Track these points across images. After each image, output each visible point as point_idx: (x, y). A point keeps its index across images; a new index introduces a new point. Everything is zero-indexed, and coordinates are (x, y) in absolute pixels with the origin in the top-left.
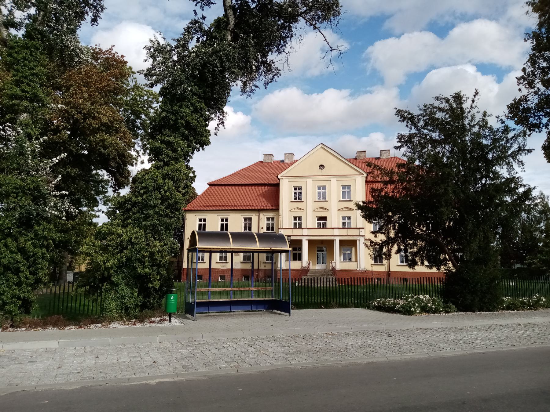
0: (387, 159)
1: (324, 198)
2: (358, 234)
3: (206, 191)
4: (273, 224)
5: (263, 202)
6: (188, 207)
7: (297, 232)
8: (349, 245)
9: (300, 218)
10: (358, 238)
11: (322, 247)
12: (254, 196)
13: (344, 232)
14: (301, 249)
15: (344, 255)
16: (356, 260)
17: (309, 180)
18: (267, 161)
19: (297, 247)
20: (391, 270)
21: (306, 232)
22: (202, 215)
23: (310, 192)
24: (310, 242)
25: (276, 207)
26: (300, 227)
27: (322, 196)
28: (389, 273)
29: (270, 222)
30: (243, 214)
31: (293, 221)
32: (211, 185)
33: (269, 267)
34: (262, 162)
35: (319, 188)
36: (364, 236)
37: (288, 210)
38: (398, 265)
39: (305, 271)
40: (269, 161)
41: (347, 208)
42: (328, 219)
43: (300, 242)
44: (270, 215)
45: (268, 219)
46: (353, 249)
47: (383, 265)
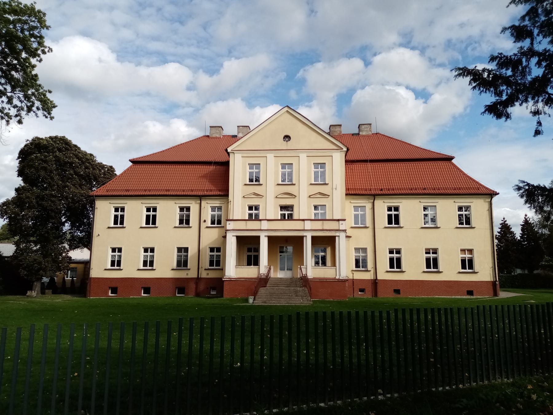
0: (368, 136)
1: (291, 180)
2: (337, 228)
3: (128, 169)
4: (220, 217)
5: (206, 186)
8: (325, 243)
9: (257, 208)
10: (337, 234)
11: (286, 246)
12: (194, 178)
13: (318, 225)
14: (257, 250)
15: (317, 257)
16: (334, 264)
17: (270, 156)
18: (214, 136)
19: (253, 247)
20: (379, 278)
21: (265, 225)
22: (119, 203)
23: (271, 172)
24: (270, 238)
25: (223, 192)
26: (257, 218)
27: (288, 179)
28: (375, 282)
29: (216, 213)
30: (177, 201)
31: (248, 212)
32: (134, 162)
33: (212, 275)
34: (208, 136)
35: (284, 166)
36: (345, 231)
37: (241, 196)
39: (263, 281)
40: (218, 136)
42: (295, 209)
43: (257, 239)
44: (216, 203)
45: (213, 209)
46: (329, 250)
47: (367, 271)
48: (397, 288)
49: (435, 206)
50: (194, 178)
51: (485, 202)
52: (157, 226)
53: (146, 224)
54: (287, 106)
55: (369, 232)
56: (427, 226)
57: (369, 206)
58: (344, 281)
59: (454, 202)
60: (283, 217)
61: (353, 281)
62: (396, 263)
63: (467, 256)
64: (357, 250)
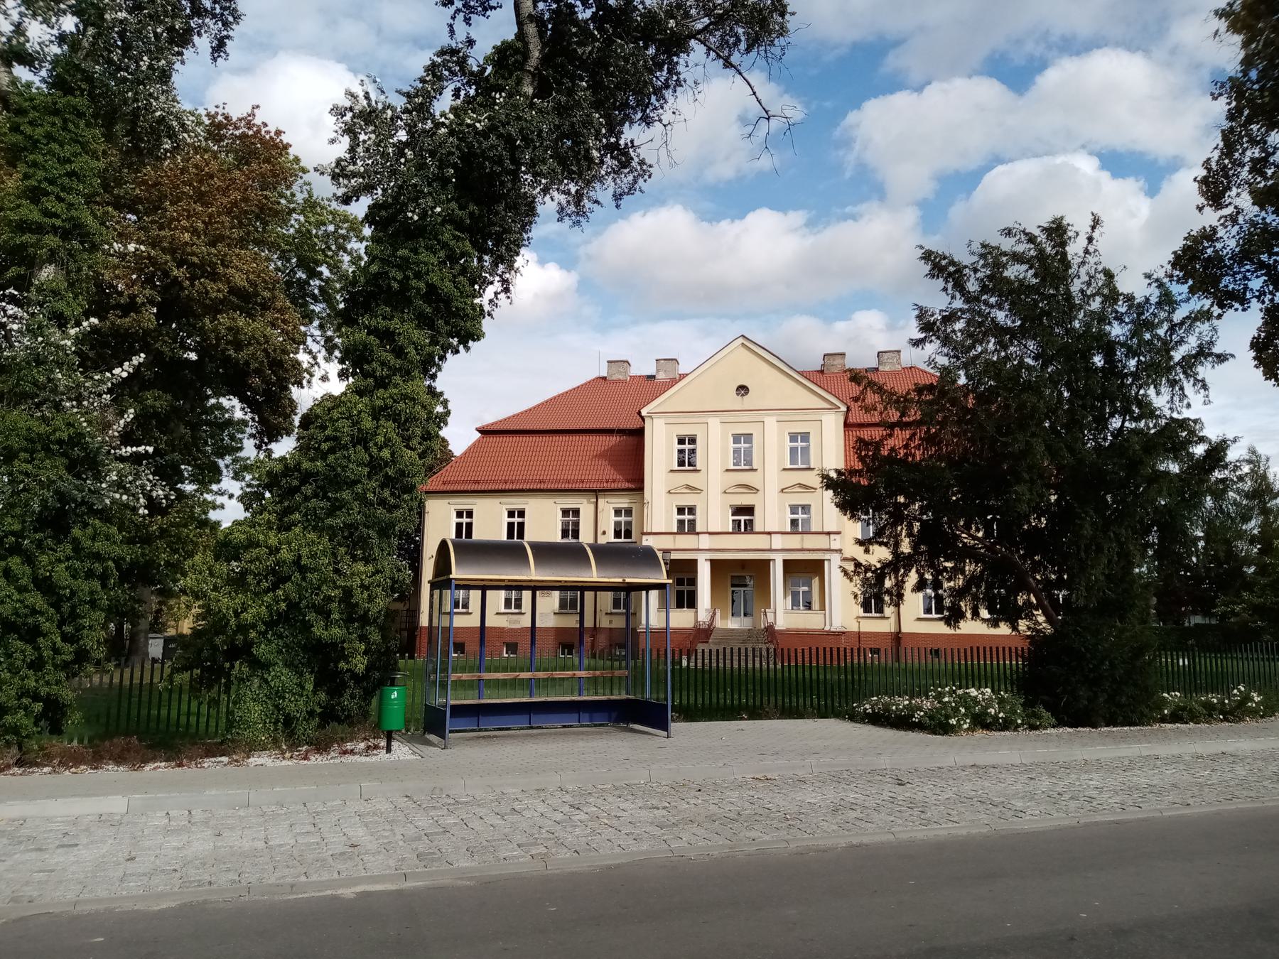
6: (431, 484)
10: (827, 556)
13: (794, 541)
21: (705, 542)
27: (744, 459)
38: (919, 619)
41: (801, 485)
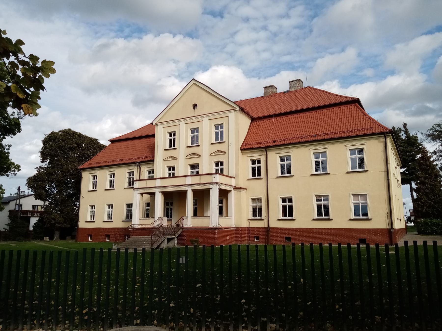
6: (85, 165)
7: (151, 183)
10: (211, 187)
13: (196, 180)
17: (182, 124)
21: (159, 183)
27: (195, 141)
28: (268, 230)
30: (127, 168)
38: (279, 220)
41: (219, 151)
48: (288, 235)
49: (326, 152)
50: (136, 149)
51: (379, 142)
52: (292, 174)
53: (253, 176)
54: (193, 79)
55: (263, 182)
56: (318, 173)
57: (263, 159)
58: (214, 230)
59: (310, 149)
60: (170, 176)
61: (249, 229)
62: (288, 212)
63: (361, 201)
64: (254, 200)
